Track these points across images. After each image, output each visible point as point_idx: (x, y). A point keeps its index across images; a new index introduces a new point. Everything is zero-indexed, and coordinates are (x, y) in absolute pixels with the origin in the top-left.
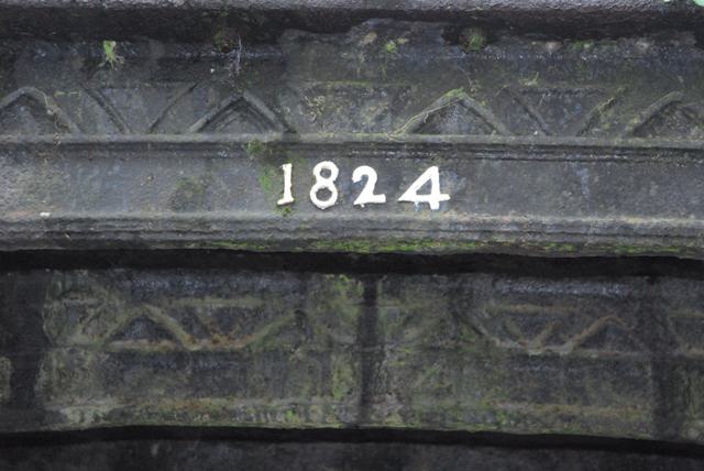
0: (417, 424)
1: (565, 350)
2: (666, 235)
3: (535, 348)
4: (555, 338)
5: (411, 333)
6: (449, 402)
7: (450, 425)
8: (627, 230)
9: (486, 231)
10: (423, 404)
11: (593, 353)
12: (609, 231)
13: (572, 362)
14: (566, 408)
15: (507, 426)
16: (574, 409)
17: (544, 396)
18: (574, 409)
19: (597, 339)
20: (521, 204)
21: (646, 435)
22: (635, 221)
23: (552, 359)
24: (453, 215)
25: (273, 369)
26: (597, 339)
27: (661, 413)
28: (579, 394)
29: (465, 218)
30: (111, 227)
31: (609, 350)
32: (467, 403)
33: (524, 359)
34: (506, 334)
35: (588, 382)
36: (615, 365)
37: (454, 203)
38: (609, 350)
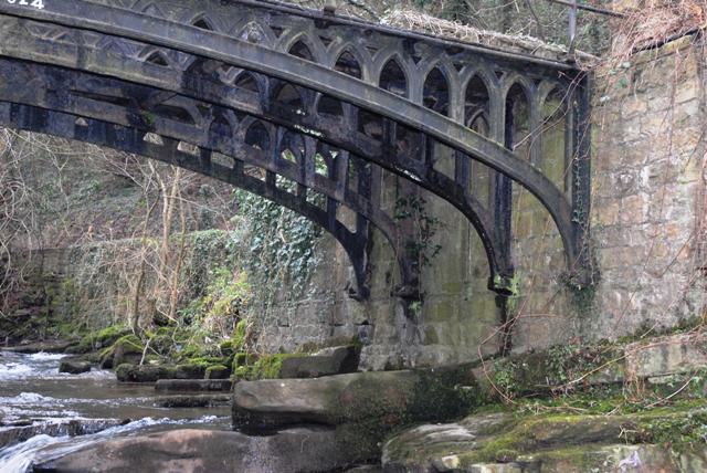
0: (6, 54)
1: (53, 39)
2: (94, 24)
3: (44, 37)
4: (50, 35)
5: (6, 27)
6: (17, 49)
7: (17, 56)
8: (87, 23)
9: (53, 16)
10: (9, 49)
11: (61, 42)
12: (212, 52)
13: (55, 43)
14: (52, 56)
15: (34, 59)
16: (54, 57)
17: (45, 51)
18: (54, 57)
19: (62, 38)
20: (61, 11)
21: (74, 67)
22: (89, 21)
23: (48, 42)
24: (44, 11)
25: (71, 332)
26: (62, 38)
27: (79, 61)
28: (55, 52)
29: (47, 12)
30: (151, 437)
31: (65, 42)
32: (22, 50)
33: (40, 40)
34: (35, 32)
35: (58, 49)
36: (67, 46)
37: (46, 7)
38: (65, 42)
